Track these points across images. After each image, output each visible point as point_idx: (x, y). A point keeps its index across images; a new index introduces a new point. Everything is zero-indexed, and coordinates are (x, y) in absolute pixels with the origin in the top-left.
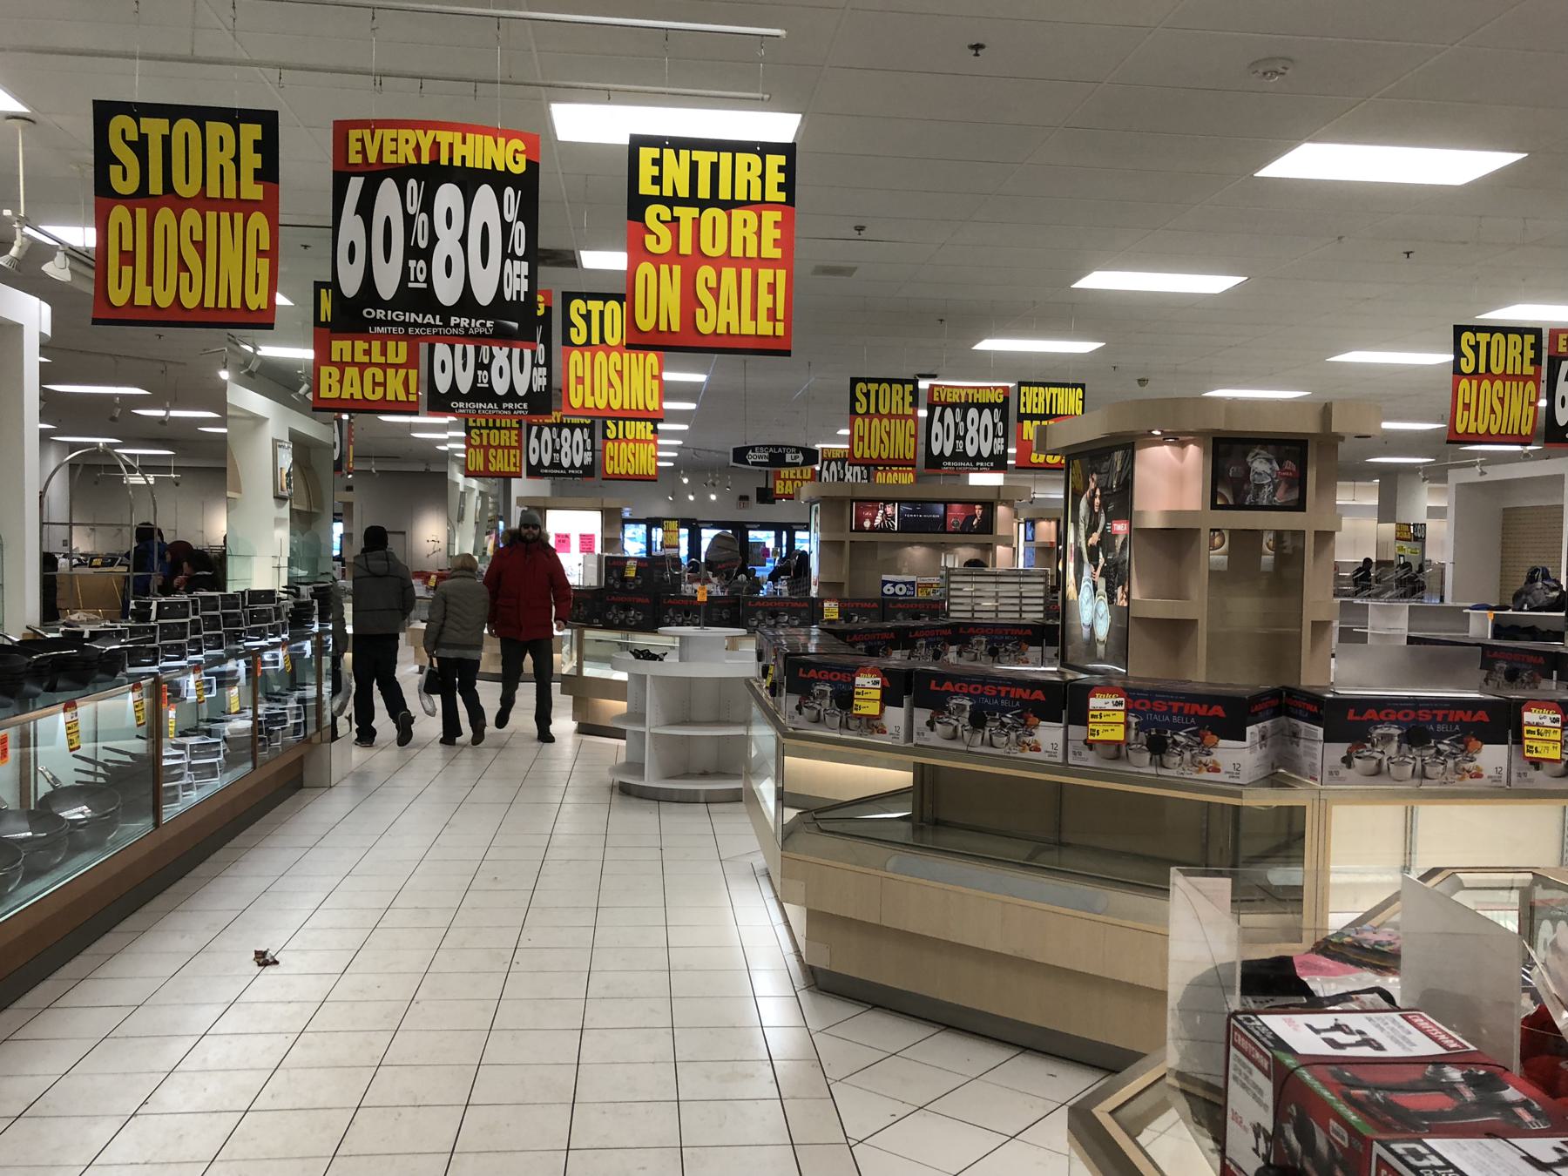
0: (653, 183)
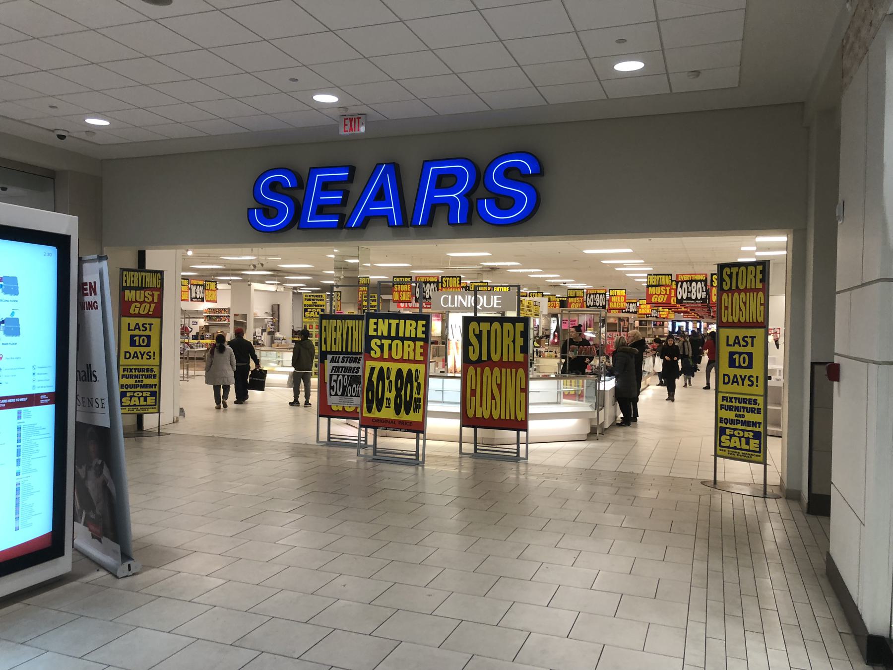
0: (374, 331)
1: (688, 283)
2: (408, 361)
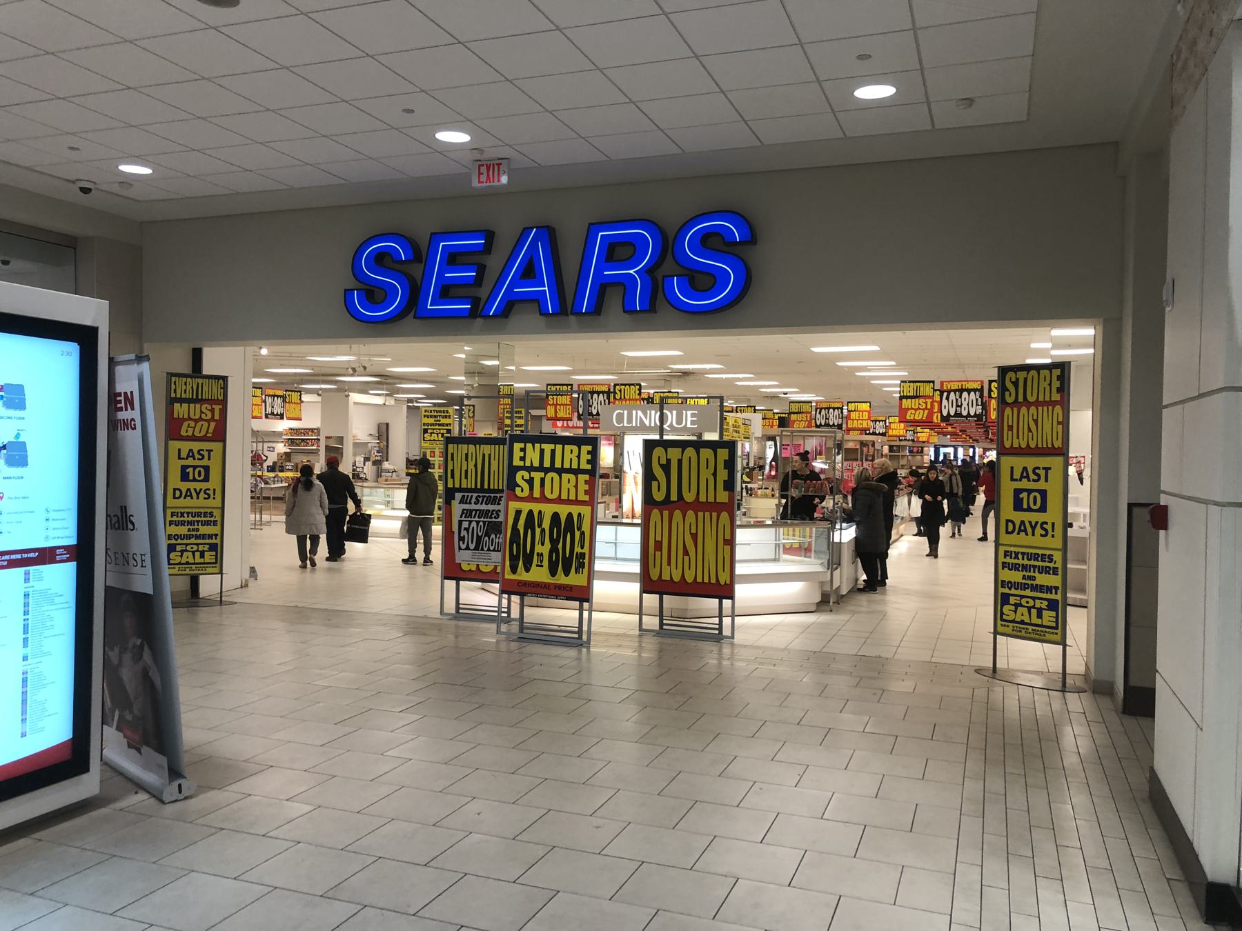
0: (520, 460)
1: (957, 393)
2: (568, 502)
